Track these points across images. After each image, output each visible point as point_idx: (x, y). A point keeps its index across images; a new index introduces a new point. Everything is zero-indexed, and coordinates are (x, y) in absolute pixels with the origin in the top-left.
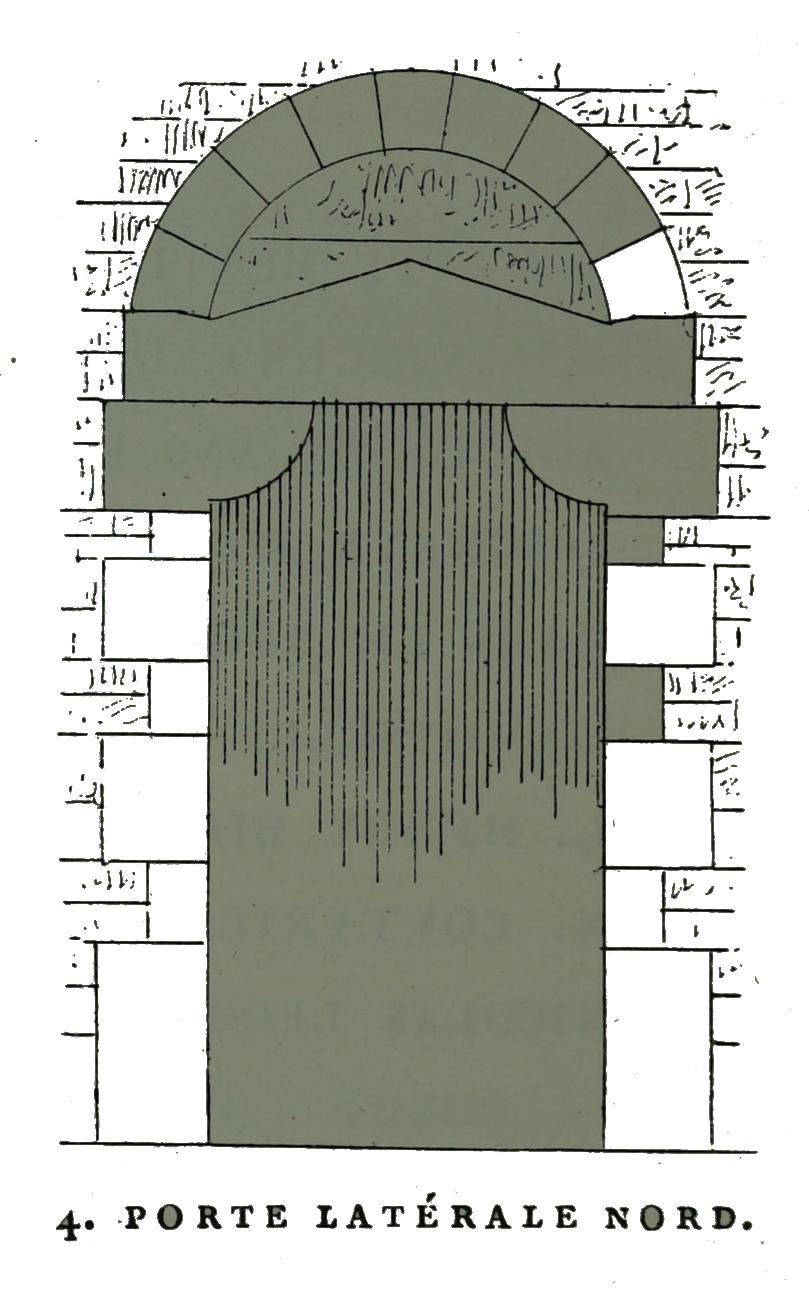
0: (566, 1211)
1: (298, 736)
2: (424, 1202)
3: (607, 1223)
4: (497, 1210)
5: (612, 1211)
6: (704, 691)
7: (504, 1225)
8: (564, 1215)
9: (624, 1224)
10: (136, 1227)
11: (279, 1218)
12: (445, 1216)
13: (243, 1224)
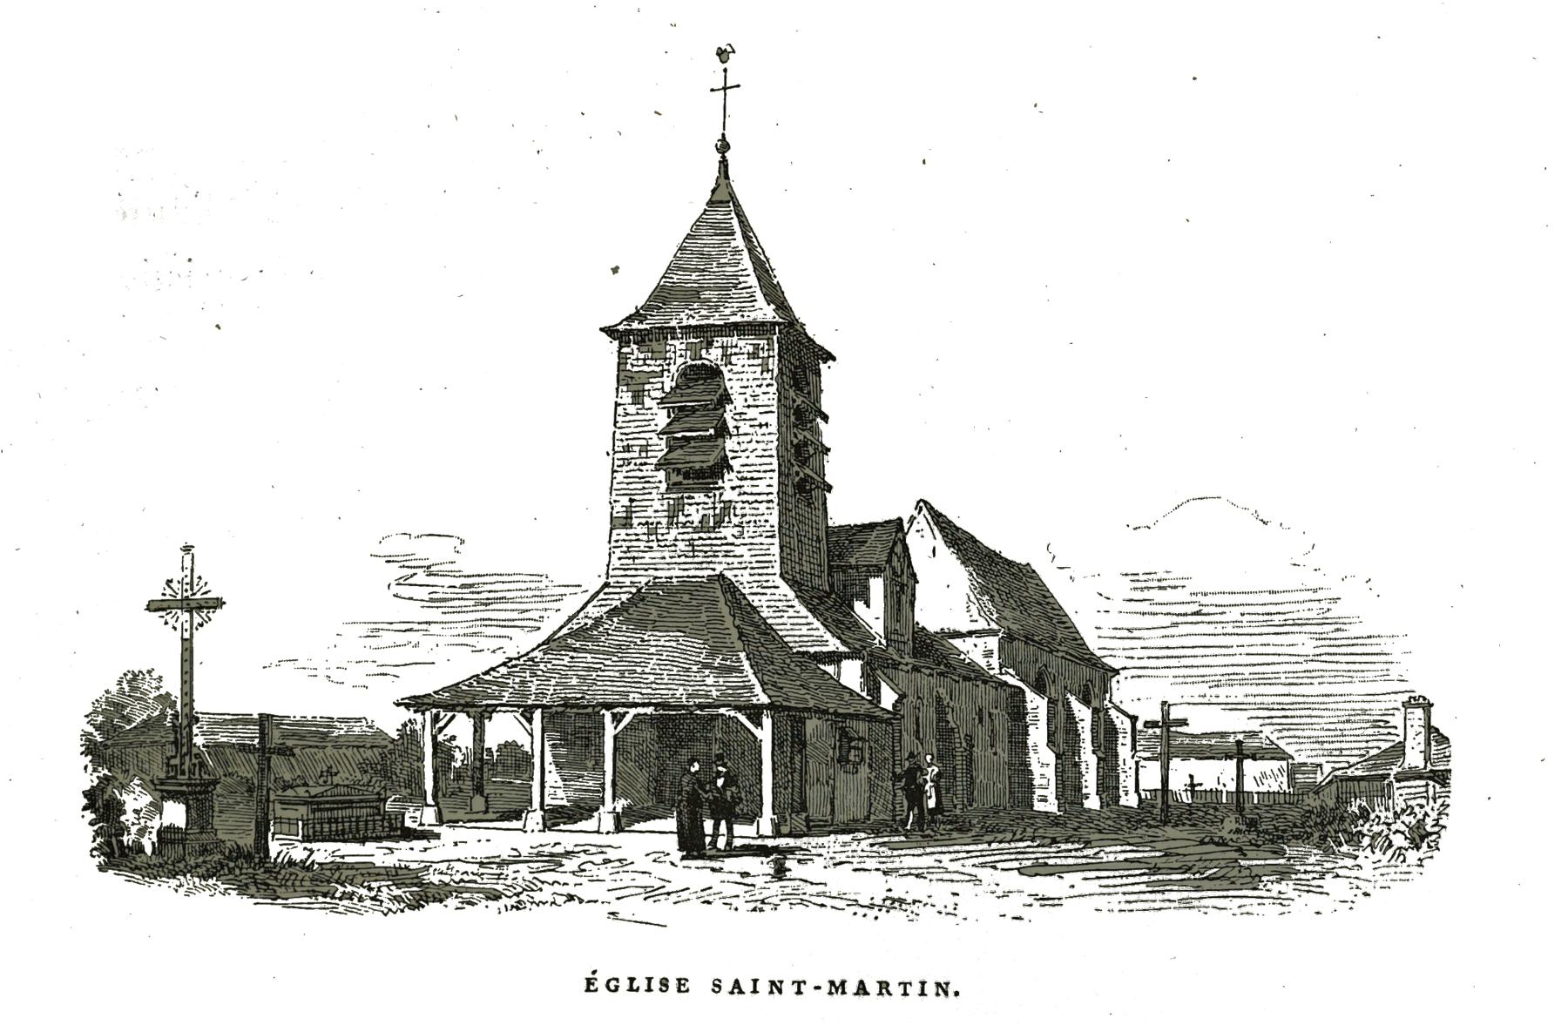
4: (737, 982)
7: (741, 992)
9: (780, 991)
13: (799, 992)
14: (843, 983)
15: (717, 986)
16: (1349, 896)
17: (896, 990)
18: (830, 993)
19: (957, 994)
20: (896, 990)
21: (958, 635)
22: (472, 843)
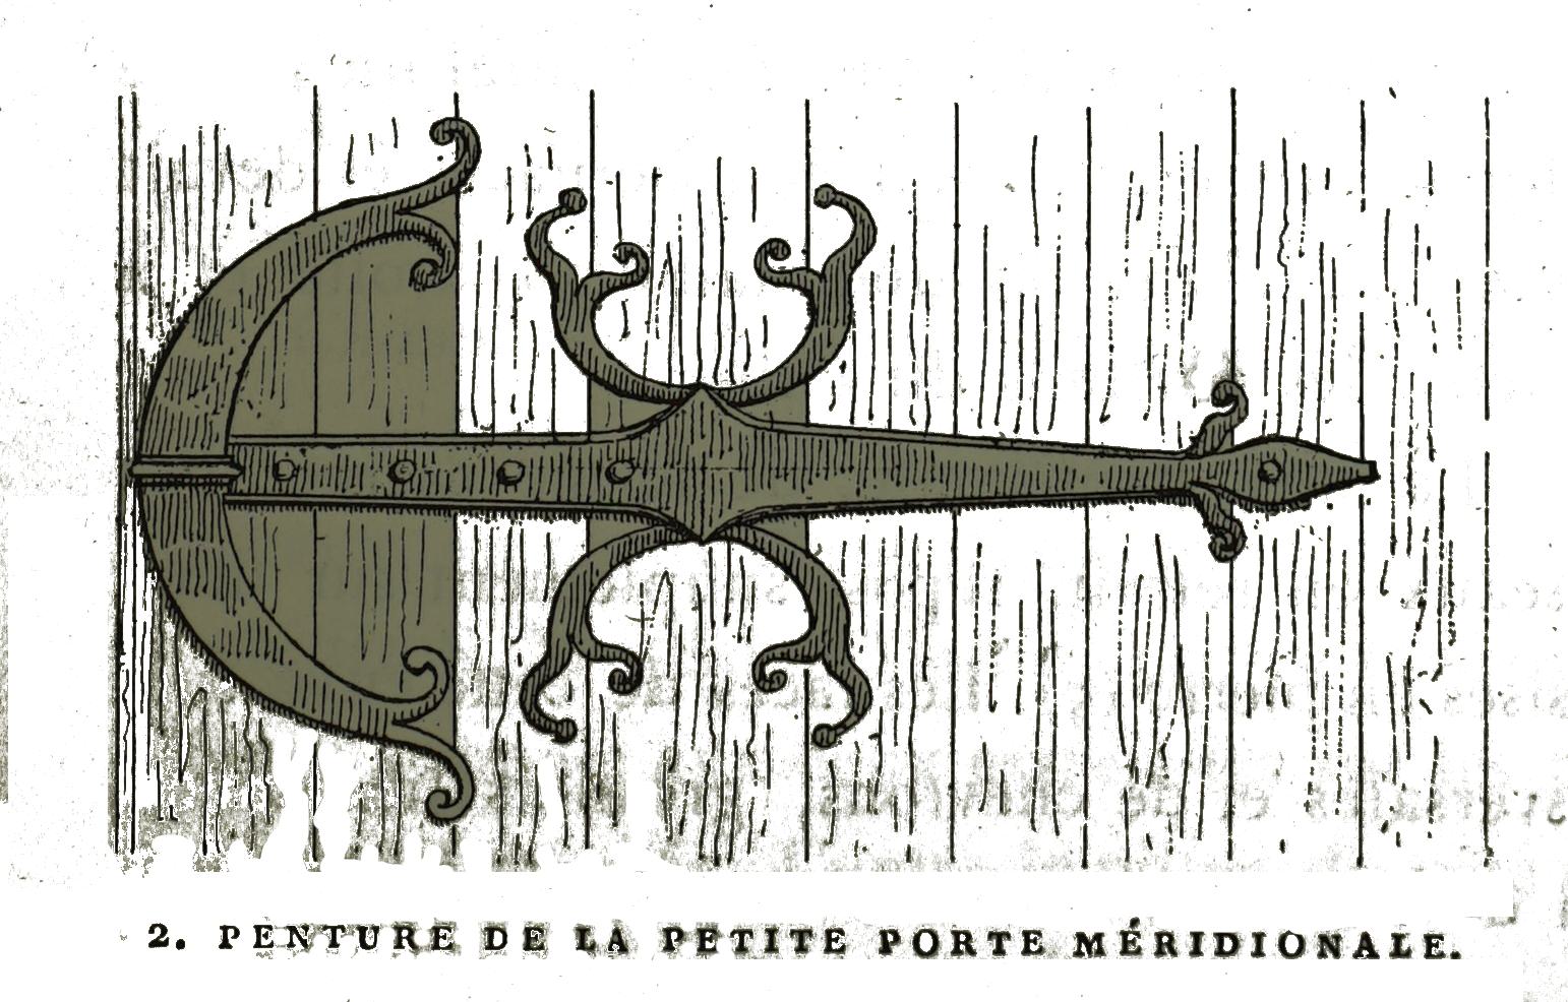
0: (1032, 936)
1: (834, 387)
2: (1126, 928)
3: (220, 942)
5: (1081, 937)
6: (197, 407)
8: (440, 936)
10: (230, 947)
11: (1035, 943)
12: (1148, 943)
14: (1099, 937)
15: (227, 937)
16: (1165, 808)
17: (982, 944)
18: (1078, 954)
19: (181, 945)
20: (982, 944)
21: (199, 279)
22: (1220, 699)
